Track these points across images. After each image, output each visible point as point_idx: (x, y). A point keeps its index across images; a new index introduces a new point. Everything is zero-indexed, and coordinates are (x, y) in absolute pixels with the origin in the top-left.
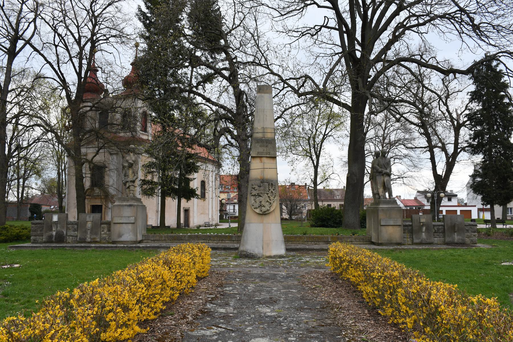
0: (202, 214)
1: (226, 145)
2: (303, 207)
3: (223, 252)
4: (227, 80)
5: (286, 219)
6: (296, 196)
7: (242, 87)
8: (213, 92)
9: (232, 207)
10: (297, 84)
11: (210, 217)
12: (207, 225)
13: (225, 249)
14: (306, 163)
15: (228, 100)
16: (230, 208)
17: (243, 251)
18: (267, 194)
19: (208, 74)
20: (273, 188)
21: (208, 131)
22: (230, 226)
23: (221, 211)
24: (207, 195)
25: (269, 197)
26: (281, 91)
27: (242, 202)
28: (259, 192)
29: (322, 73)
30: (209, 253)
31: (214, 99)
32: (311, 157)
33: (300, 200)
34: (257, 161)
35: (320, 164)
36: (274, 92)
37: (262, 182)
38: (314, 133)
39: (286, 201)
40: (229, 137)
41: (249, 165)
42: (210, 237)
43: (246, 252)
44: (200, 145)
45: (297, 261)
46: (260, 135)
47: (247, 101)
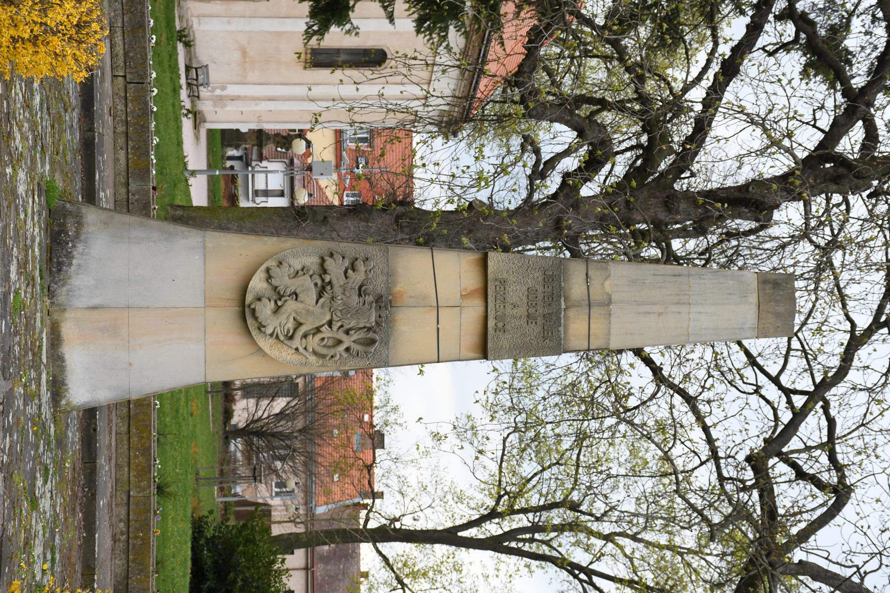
0: (244, 53)
1: (537, 152)
2: (281, 484)
3: (72, 138)
4: (821, 145)
5: (228, 414)
6: (327, 453)
7: (789, 215)
8: (769, 87)
9: (276, 181)
10: (808, 449)
11: (232, 90)
12: (197, 76)
13: (89, 148)
14: (469, 492)
15: (730, 155)
16: (269, 177)
17: (80, 224)
18: (330, 323)
19: (847, 57)
20: (356, 347)
21: (596, 73)
22: (193, 173)
23: (260, 137)
24: (324, 74)
25: (318, 330)
26: (776, 380)
27: (298, 219)
28: (337, 290)
29: (858, 560)
30: (63, 71)
31: (736, 91)
32: (493, 514)
33: (310, 474)
34: (470, 279)
35: (466, 555)
36: (767, 348)
37: (379, 299)
38: (595, 526)
39: (305, 413)
40: (570, 164)
41: (453, 244)
42: (141, 81)
43: (77, 236)
44: (535, 37)
45: (37, 458)
46: (576, 287)
47: (730, 235)
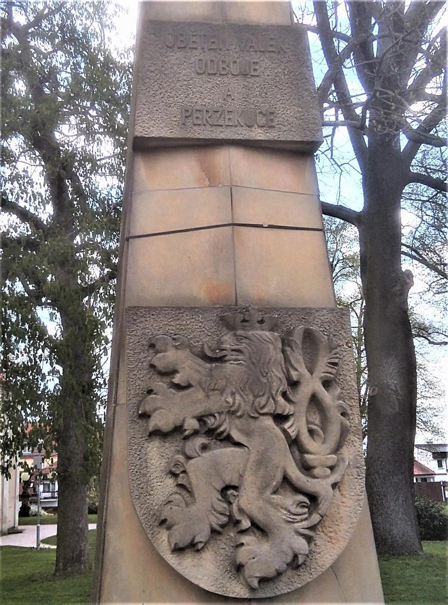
18: (280, 418)
20: (322, 367)
25: (295, 443)
28: (215, 403)
